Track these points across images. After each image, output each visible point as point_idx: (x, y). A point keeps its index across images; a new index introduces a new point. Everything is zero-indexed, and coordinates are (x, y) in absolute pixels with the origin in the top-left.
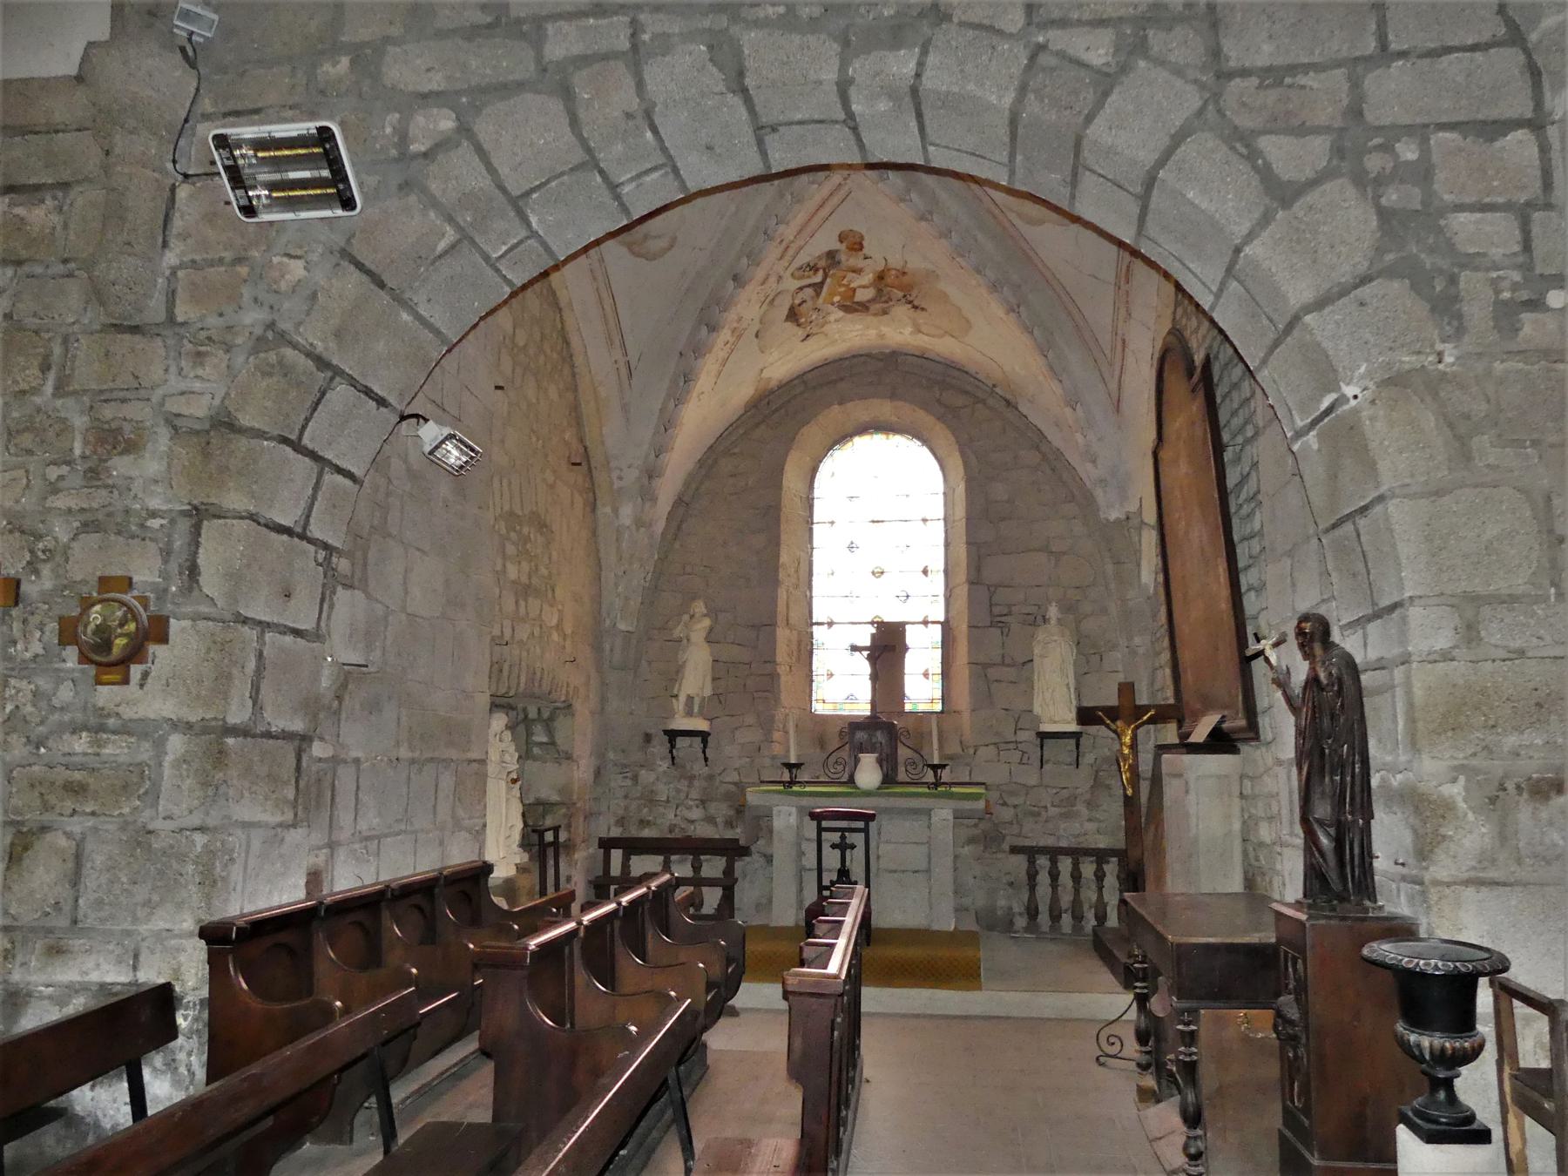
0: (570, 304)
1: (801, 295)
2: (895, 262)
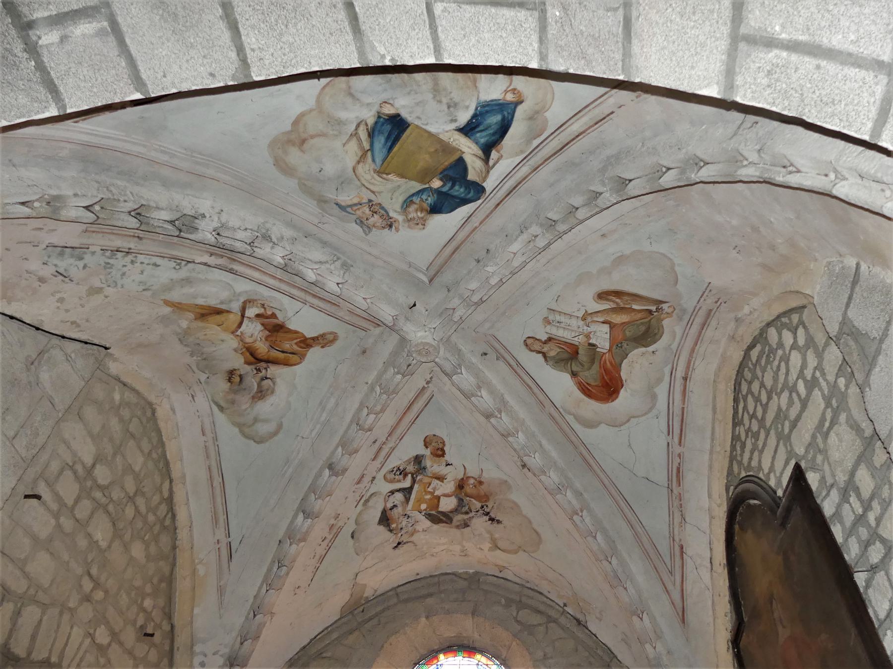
0: (184, 476)
1: (392, 499)
2: (473, 471)
